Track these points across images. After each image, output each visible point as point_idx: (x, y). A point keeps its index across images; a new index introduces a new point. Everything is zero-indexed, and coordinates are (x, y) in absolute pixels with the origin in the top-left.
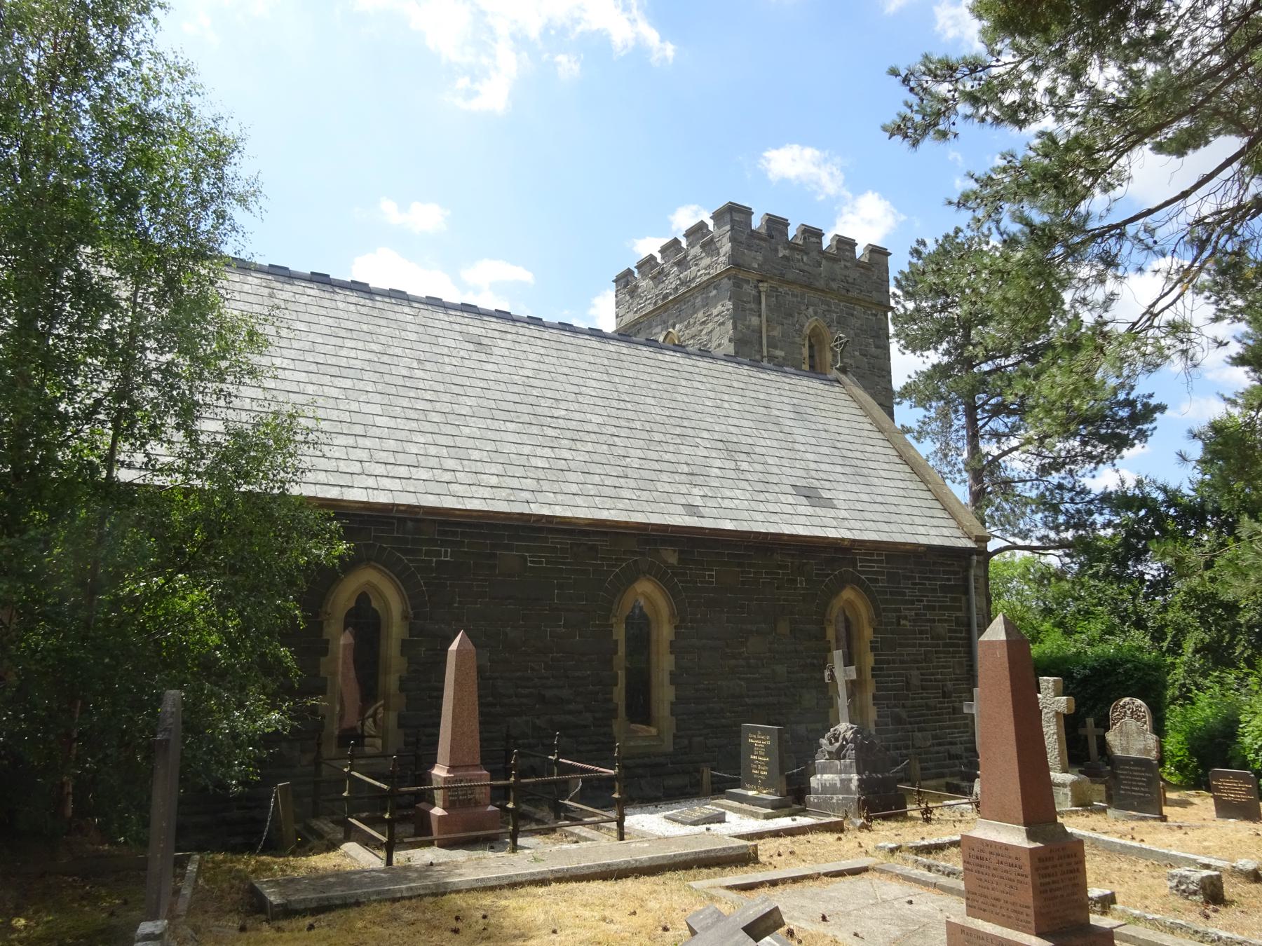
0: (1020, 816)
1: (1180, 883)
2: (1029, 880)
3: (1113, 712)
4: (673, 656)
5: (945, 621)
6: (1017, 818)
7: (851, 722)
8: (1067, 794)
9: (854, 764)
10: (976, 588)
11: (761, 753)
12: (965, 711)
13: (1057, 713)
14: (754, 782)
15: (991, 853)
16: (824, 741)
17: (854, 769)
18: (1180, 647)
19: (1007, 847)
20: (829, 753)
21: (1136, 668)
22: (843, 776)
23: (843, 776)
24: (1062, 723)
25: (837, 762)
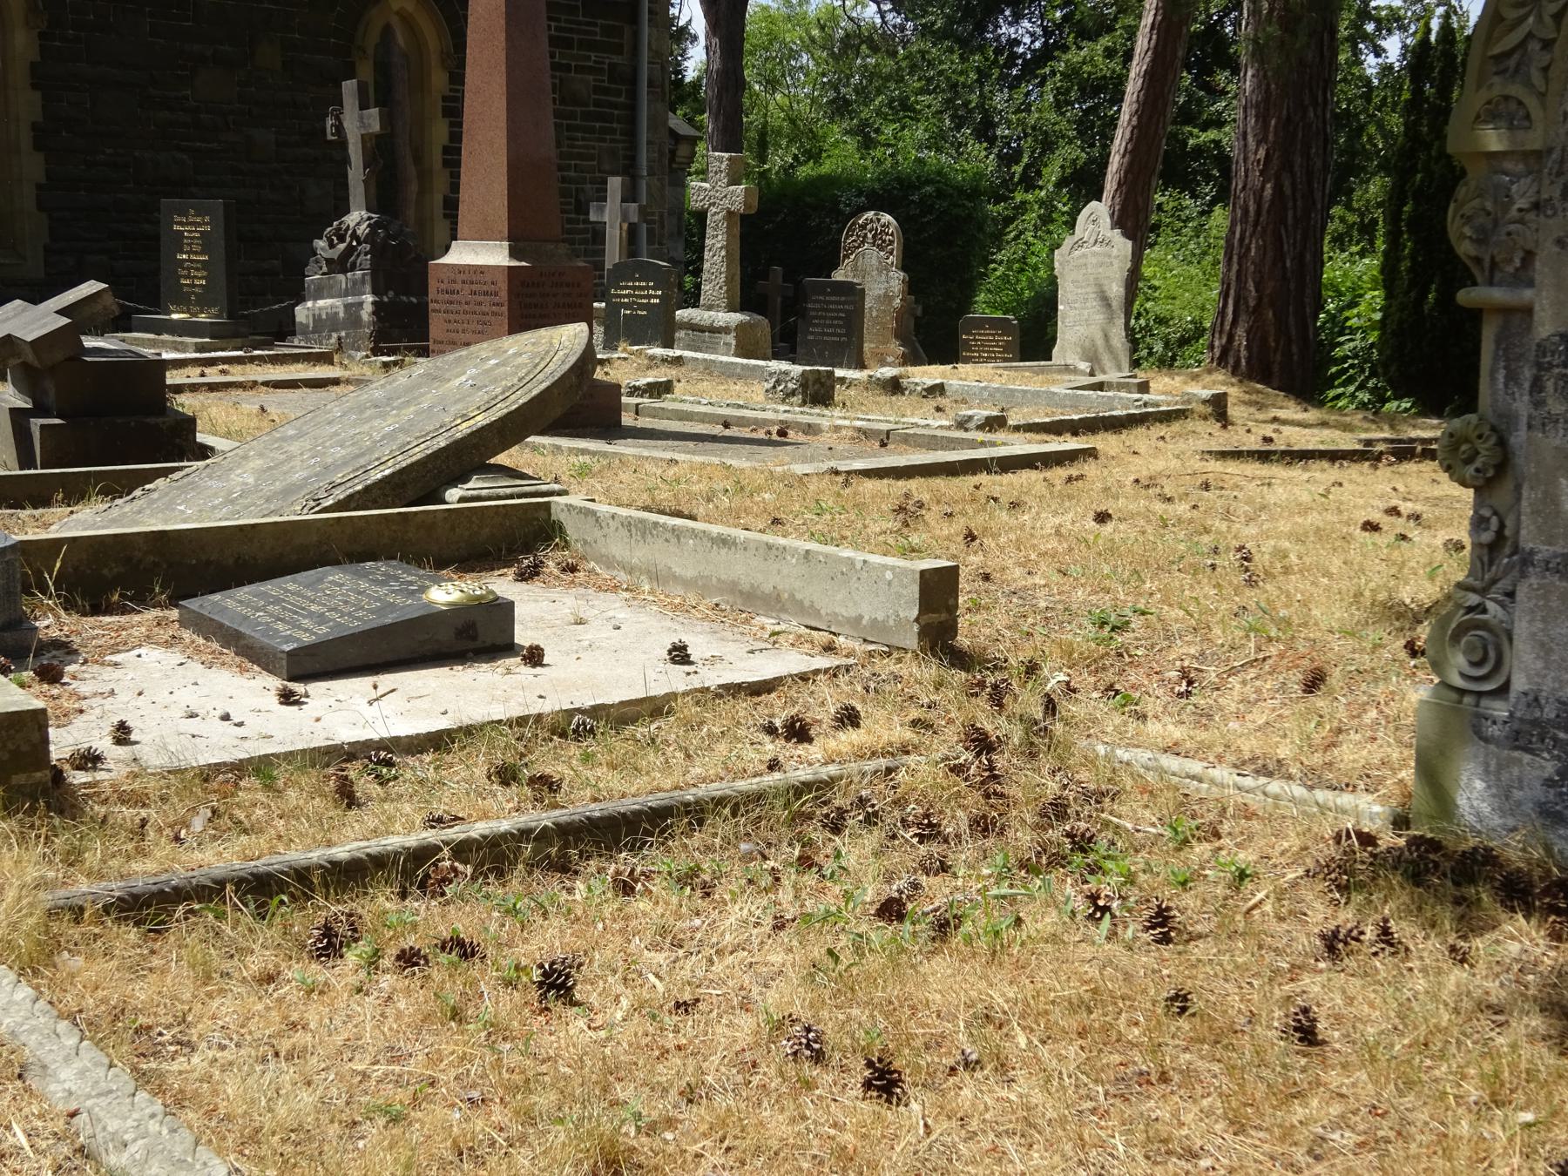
0: (505, 229)
1: (778, 382)
2: (505, 309)
3: (846, 238)
4: (38, 95)
5: (591, 70)
6: (500, 232)
7: (368, 210)
8: (730, 344)
9: (368, 278)
10: (650, 12)
11: (195, 248)
12: (593, 217)
13: (730, 213)
14: (182, 301)
15: (464, 282)
16: (320, 244)
17: (368, 288)
18: (1039, 174)
19: (481, 270)
20: (329, 261)
21: (940, 194)
22: (350, 299)
23: (350, 299)
24: (737, 230)
25: (341, 277)
